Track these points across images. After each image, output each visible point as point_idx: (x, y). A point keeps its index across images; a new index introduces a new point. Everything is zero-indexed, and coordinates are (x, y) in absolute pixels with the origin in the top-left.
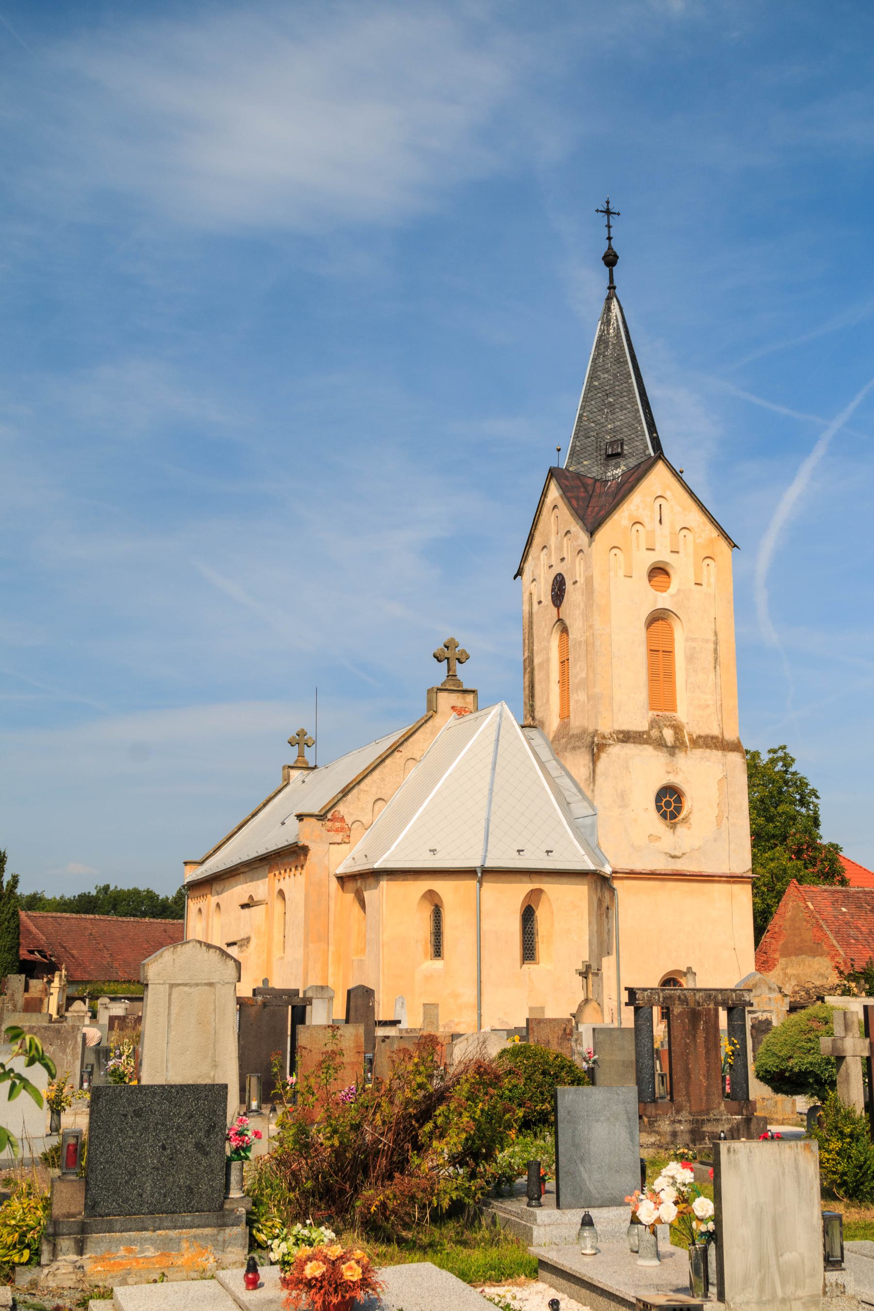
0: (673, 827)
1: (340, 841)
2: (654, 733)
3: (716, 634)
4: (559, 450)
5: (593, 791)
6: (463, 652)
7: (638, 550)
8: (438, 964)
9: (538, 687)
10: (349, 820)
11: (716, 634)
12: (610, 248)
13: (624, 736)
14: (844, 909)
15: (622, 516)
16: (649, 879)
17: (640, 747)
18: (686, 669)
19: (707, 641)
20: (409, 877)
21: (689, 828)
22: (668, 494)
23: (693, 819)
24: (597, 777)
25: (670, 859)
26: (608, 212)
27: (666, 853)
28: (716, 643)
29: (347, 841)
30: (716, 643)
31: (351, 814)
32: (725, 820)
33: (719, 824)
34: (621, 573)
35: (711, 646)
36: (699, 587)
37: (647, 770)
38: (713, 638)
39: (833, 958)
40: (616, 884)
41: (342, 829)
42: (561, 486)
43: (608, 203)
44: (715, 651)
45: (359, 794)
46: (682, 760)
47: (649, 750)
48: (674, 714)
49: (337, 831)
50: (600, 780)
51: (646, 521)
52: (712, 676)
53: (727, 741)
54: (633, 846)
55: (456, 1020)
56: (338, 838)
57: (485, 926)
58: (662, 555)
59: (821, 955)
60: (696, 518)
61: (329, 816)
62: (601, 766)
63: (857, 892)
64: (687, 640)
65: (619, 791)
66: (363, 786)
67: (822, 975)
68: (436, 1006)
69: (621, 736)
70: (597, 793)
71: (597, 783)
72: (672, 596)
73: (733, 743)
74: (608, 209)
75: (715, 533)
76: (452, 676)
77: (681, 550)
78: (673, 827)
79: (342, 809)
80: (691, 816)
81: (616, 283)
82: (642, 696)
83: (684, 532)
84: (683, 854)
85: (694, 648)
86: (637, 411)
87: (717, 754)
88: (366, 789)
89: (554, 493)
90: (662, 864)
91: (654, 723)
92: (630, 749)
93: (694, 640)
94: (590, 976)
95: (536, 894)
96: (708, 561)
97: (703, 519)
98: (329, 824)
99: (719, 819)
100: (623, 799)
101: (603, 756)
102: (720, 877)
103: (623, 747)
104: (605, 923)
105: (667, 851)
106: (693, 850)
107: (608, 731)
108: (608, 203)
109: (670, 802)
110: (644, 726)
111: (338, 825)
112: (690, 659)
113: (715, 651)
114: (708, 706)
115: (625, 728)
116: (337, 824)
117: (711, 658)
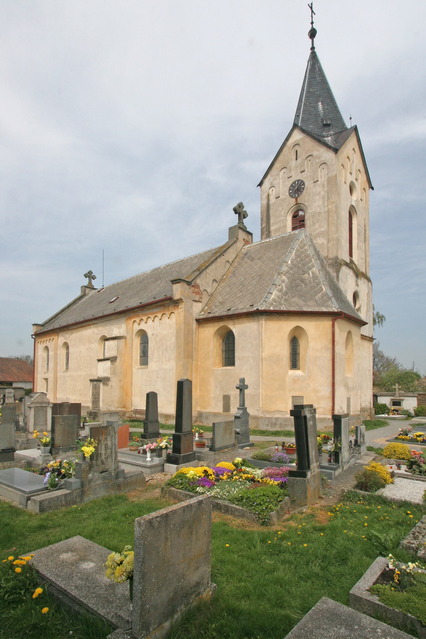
31: (203, 286)
98: (193, 288)
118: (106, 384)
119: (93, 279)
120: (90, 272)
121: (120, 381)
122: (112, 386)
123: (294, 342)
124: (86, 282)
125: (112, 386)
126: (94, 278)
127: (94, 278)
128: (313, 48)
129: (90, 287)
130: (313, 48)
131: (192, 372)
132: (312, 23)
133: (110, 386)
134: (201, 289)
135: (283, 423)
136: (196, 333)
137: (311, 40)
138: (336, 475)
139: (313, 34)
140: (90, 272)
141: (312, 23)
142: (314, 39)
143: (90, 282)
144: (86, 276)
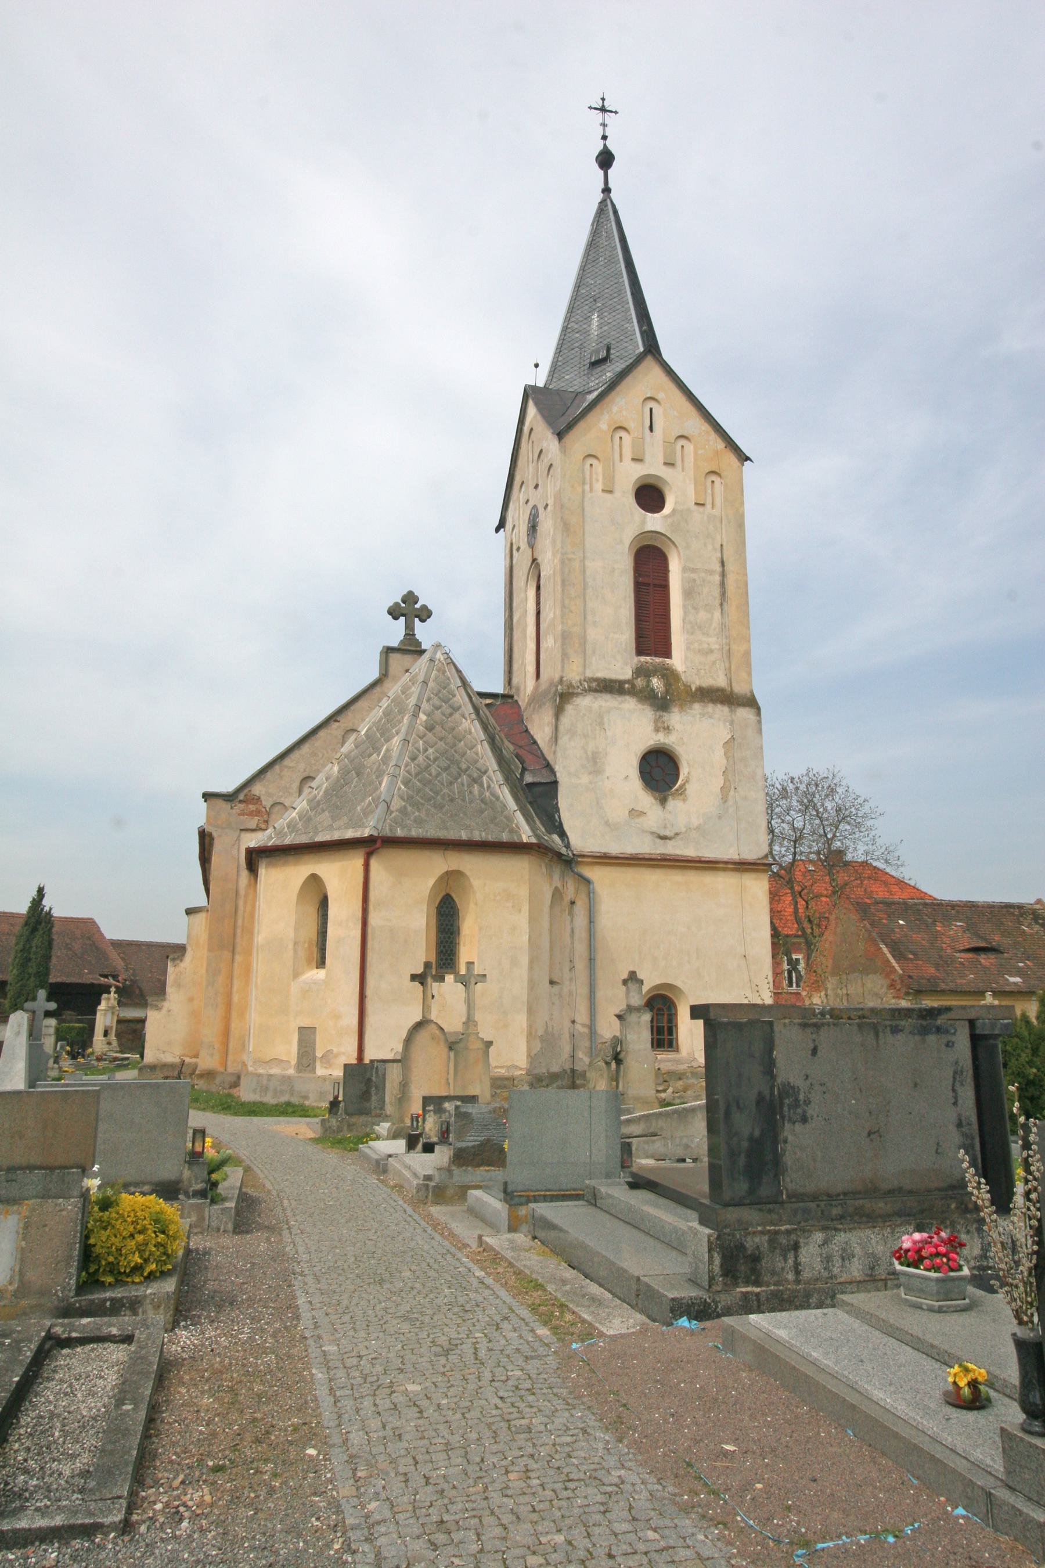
0: (663, 801)
1: (254, 827)
2: (640, 682)
3: (723, 563)
4: (537, 366)
5: (555, 752)
6: (424, 607)
7: (621, 460)
8: (321, 974)
9: (516, 649)
10: (267, 803)
11: (723, 563)
12: (605, 145)
13: (598, 685)
14: (901, 922)
15: (601, 422)
16: (629, 865)
17: (620, 699)
18: (684, 606)
19: (711, 572)
20: (291, 858)
21: (684, 800)
22: (660, 396)
23: (691, 789)
24: (560, 736)
25: (658, 841)
26: (603, 110)
27: (652, 833)
28: (723, 575)
29: (263, 826)
30: (723, 575)
31: (269, 795)
32: (732, 793)
33: (725, 799)
34: (599, 486)
35: (717, 578)
36: (701, 509)
37: (631, 729)
38: (718, 568)
39: (887, 976)
40: (596, 874)
41: (258, 813)
42: (536, 404)
43: (603, 99)
44: (723, 584)
45: (281, 771)
46: (675, 718)
47: (630, 703)
48: (668, 661)
49: (251, 814)
50: (563, 740)
51: (631, 425)
52: (717, 614)
53: (736, 694)
54: (607, 823)
55: (335, 1050)
56: (253, 823)
57: (373, 920)
58: (653, 467)
59: (875, 973)
60: (695, 425)
61: (241, 797)
62: (565, 721)
63: (916, 904)
64: (685, 569)
65: (589, 753)
66: (287, 762)
67: (876, 994)
68: (313, 1029)
69: (594, 685)
70: (559, 754)
71: (560, 742)
72: (666, 517)
73: (744, 697)
74: (603, 106)
75: (720, 445)
76: (410, 633)
77: (679, 463)
78: (663, 801)
79: (257, 789)
80: (687, 786)
81: (611, 185)
82: (627, 635)
83: (682, 442)
84: (677, 834)
85: (694, 580)
86: (629, 310)
87: (721, 711)
88: (292, 765)
89: (532, 410)
90: (645, 847)
91: (641, 672)
92: (606, 702)
93: (694, 570)
94: (429, 980)
95: (452, 877)
96: (713, 478)
97: (706, 427)
98: (242, 806)
99: (725, 790)
100: (595, 763)
101: (569, 709)
102: (726, 863)
103: (596, 698)
104: (568, 923)
105: (654, 829)
106: (689, 829)
107: (578, 678)
108: (603, 99)
109: (659, 770)
110: (626, 674)
111: (252, 807)
112: (688, 593)
113: (723, 584)
114: (712, 651)
115: (600, 675)
116: (251, 806)
117: (716, 592)
118: (156, 1006)
119: (423, 621)
120: (410, 598)
121: (191, 1000)
122: (169, 1011)
123: (447, 917)
124: (395, 632)
125: (169, 1011)
126: (425, 614)
127: (425, 614)
128: (607, 190)
129: (411, 647)
130: (607, 190)
131: (231, 977)
132: (604, 138)
133: (164, 1011)
134: (264, 803)
135: (279, 1088)
136: (246, 895)
137: (602, 172)
138: (998, 1466)
139: (606, 160)
140: (410, 598)
141: (604, 138)
142: (609, 171)
143: (410, 633)
144: (395, 613)
